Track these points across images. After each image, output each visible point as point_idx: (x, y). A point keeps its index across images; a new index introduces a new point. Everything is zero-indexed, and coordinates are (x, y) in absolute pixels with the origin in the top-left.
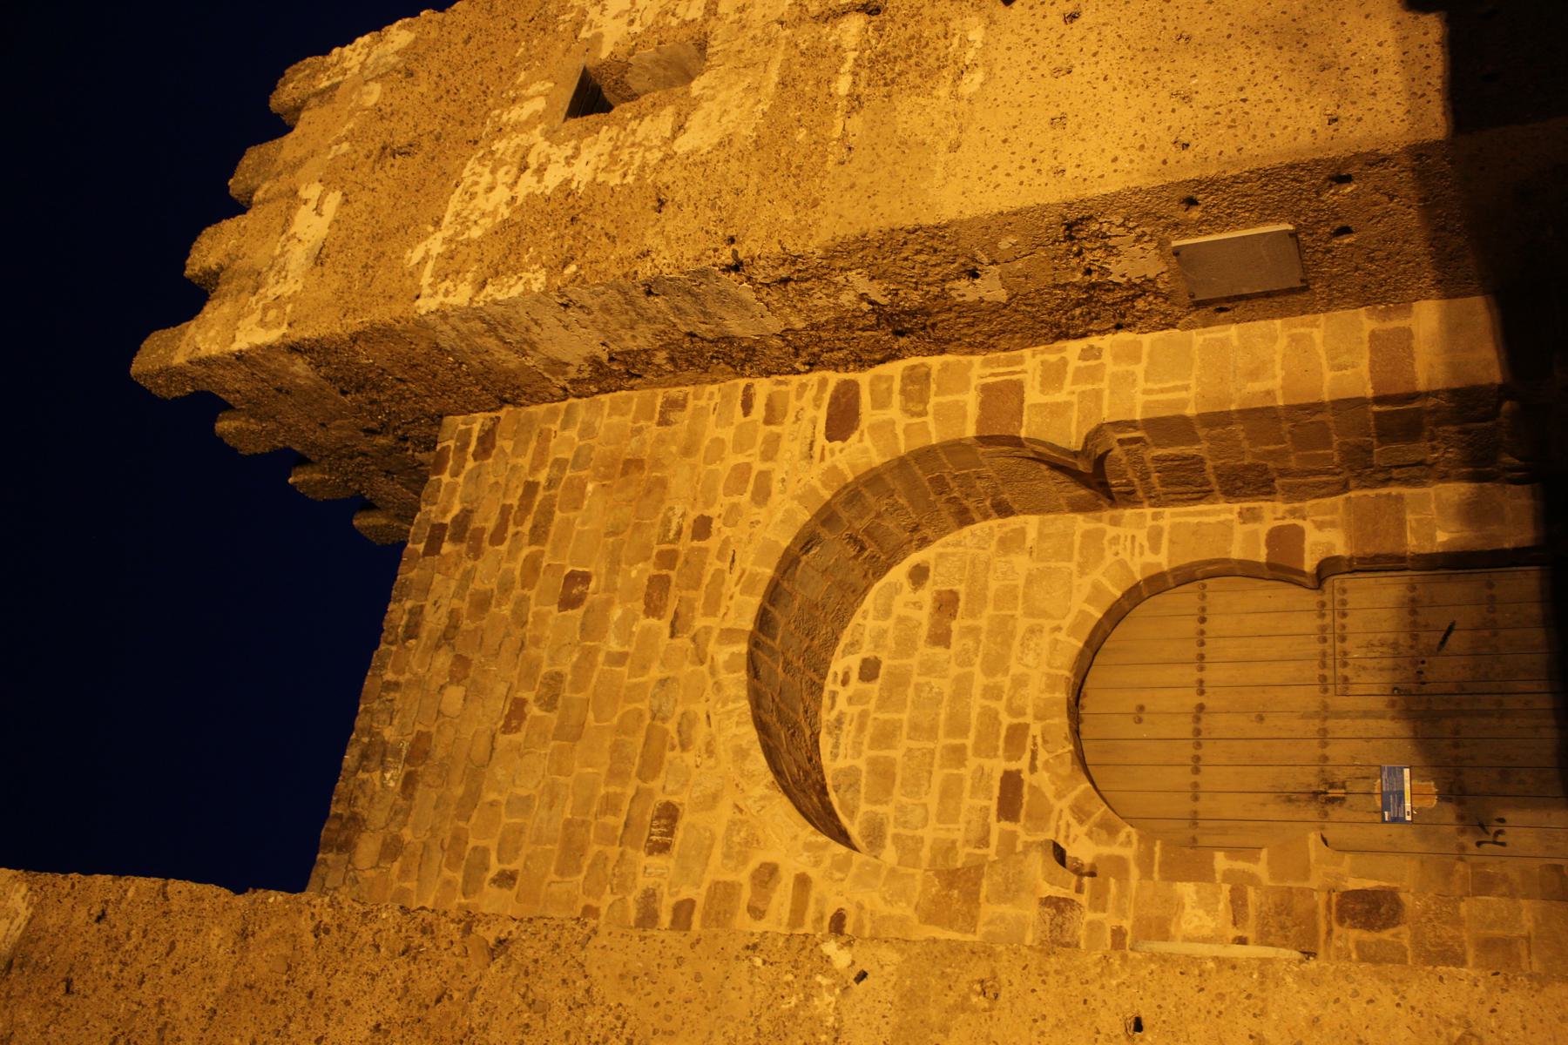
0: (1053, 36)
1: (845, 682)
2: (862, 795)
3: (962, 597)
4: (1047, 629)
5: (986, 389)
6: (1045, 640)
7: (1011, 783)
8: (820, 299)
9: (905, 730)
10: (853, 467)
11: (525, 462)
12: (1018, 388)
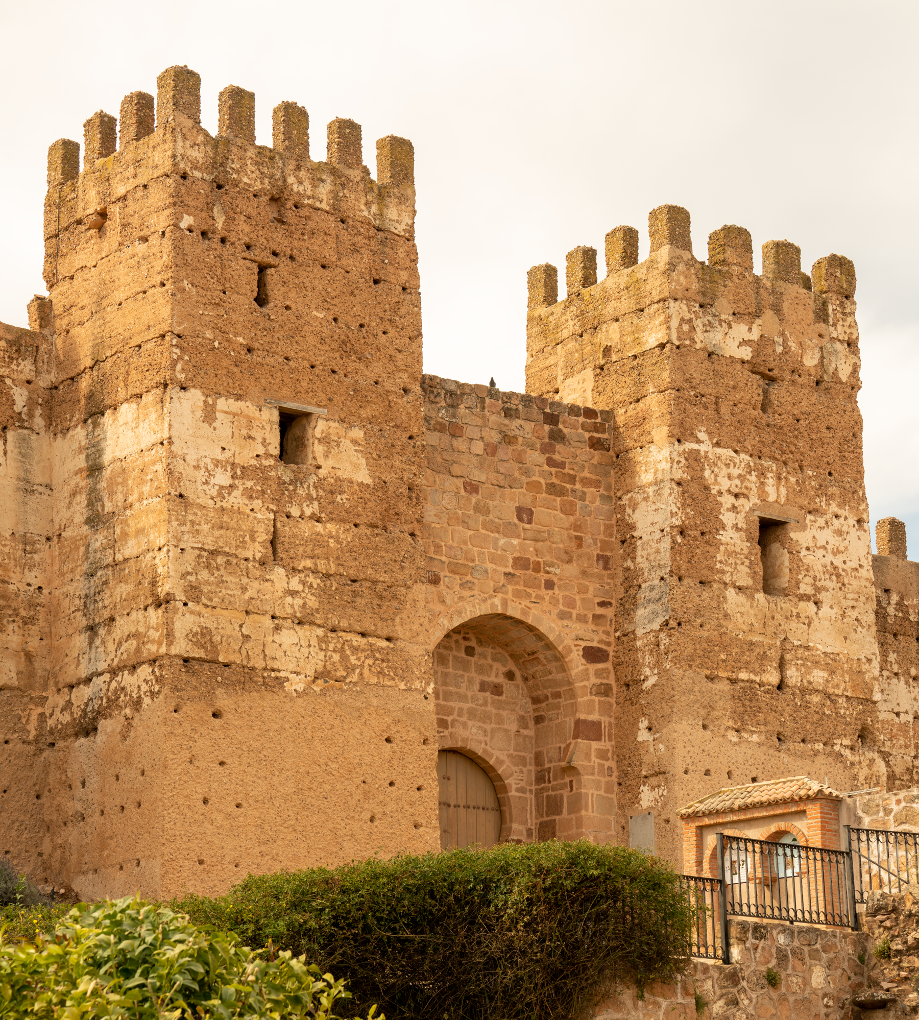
0: (748, 772)
1: (465, 638)
3: (500, 698)
4: (486, 739)
5: (599, 723)
6: (482, 738)
8: (648, 659)
10: (571, 661)
11: (586, 474)
12: (598, 738)
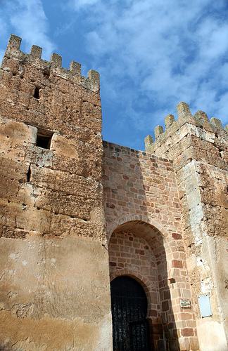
12: (182, 267)
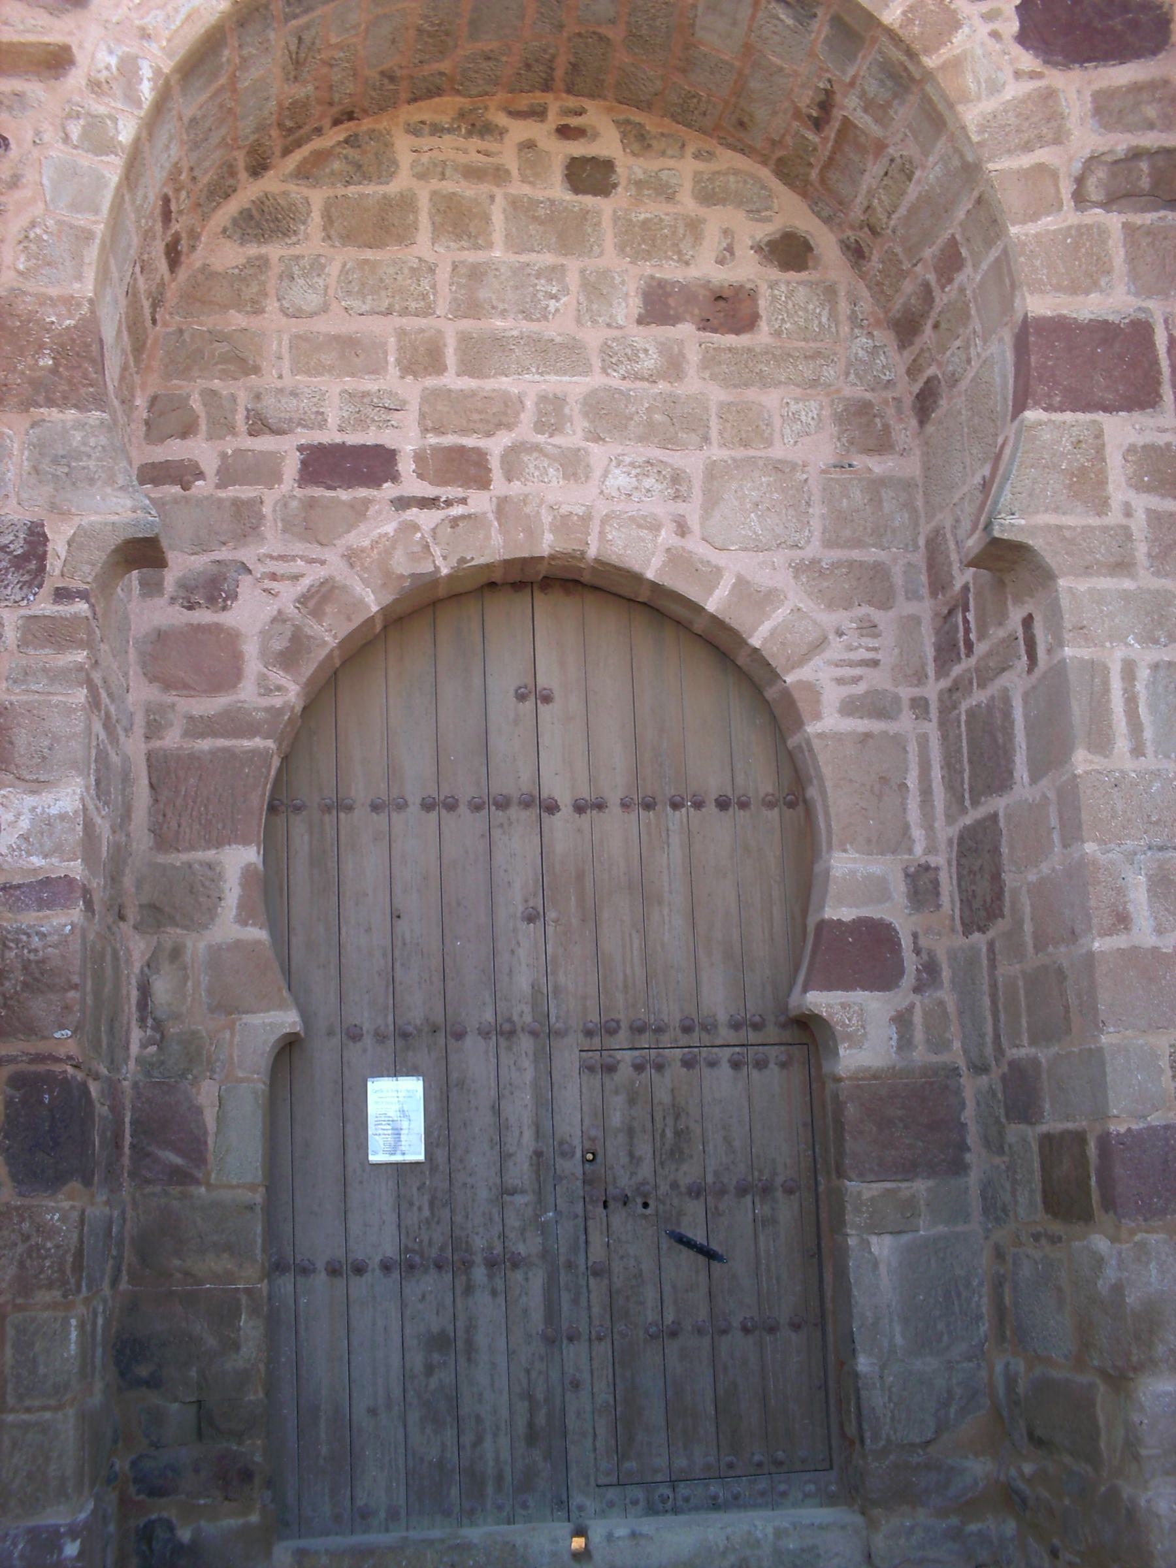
1: (565, 132)
2: (341, 191)
3: (744, 340)
4: (681, 508)
5: (1141, 330)
6: (659, 507)
7: (374, 465)
9: (472, 257)
10: (956, 64)
